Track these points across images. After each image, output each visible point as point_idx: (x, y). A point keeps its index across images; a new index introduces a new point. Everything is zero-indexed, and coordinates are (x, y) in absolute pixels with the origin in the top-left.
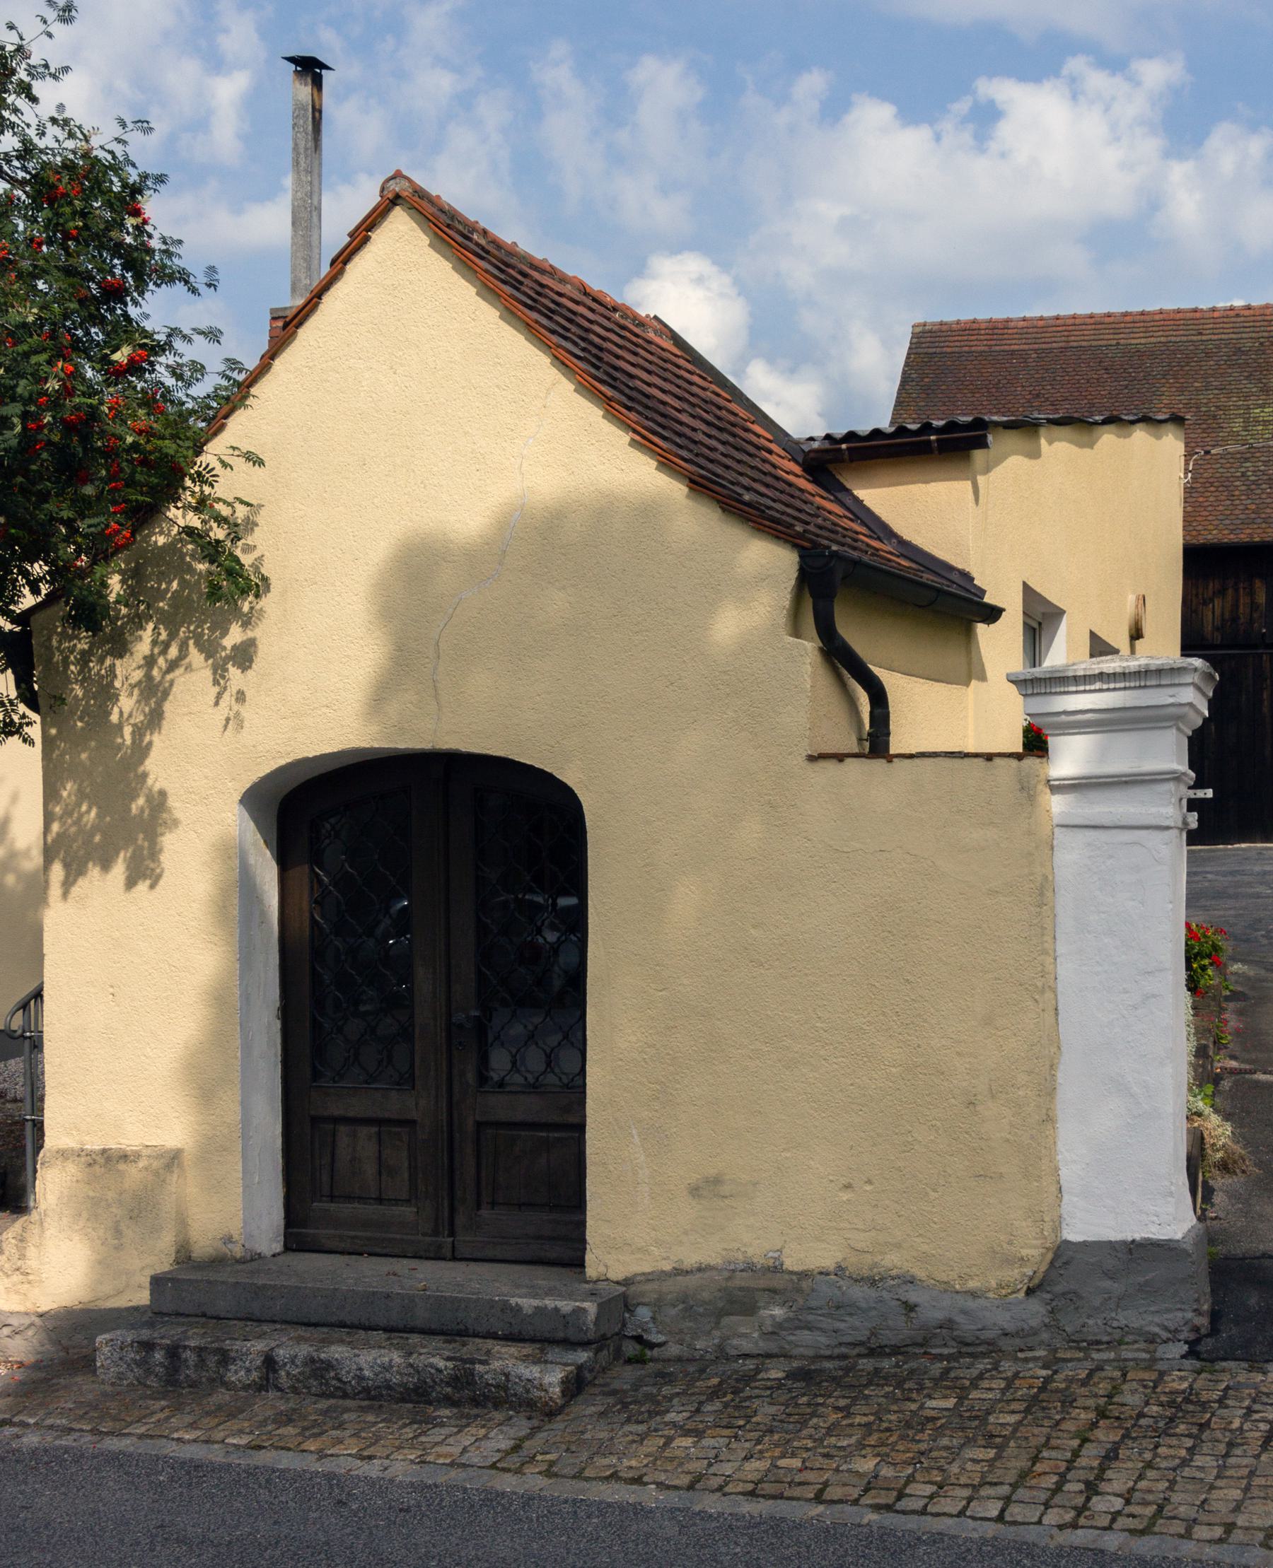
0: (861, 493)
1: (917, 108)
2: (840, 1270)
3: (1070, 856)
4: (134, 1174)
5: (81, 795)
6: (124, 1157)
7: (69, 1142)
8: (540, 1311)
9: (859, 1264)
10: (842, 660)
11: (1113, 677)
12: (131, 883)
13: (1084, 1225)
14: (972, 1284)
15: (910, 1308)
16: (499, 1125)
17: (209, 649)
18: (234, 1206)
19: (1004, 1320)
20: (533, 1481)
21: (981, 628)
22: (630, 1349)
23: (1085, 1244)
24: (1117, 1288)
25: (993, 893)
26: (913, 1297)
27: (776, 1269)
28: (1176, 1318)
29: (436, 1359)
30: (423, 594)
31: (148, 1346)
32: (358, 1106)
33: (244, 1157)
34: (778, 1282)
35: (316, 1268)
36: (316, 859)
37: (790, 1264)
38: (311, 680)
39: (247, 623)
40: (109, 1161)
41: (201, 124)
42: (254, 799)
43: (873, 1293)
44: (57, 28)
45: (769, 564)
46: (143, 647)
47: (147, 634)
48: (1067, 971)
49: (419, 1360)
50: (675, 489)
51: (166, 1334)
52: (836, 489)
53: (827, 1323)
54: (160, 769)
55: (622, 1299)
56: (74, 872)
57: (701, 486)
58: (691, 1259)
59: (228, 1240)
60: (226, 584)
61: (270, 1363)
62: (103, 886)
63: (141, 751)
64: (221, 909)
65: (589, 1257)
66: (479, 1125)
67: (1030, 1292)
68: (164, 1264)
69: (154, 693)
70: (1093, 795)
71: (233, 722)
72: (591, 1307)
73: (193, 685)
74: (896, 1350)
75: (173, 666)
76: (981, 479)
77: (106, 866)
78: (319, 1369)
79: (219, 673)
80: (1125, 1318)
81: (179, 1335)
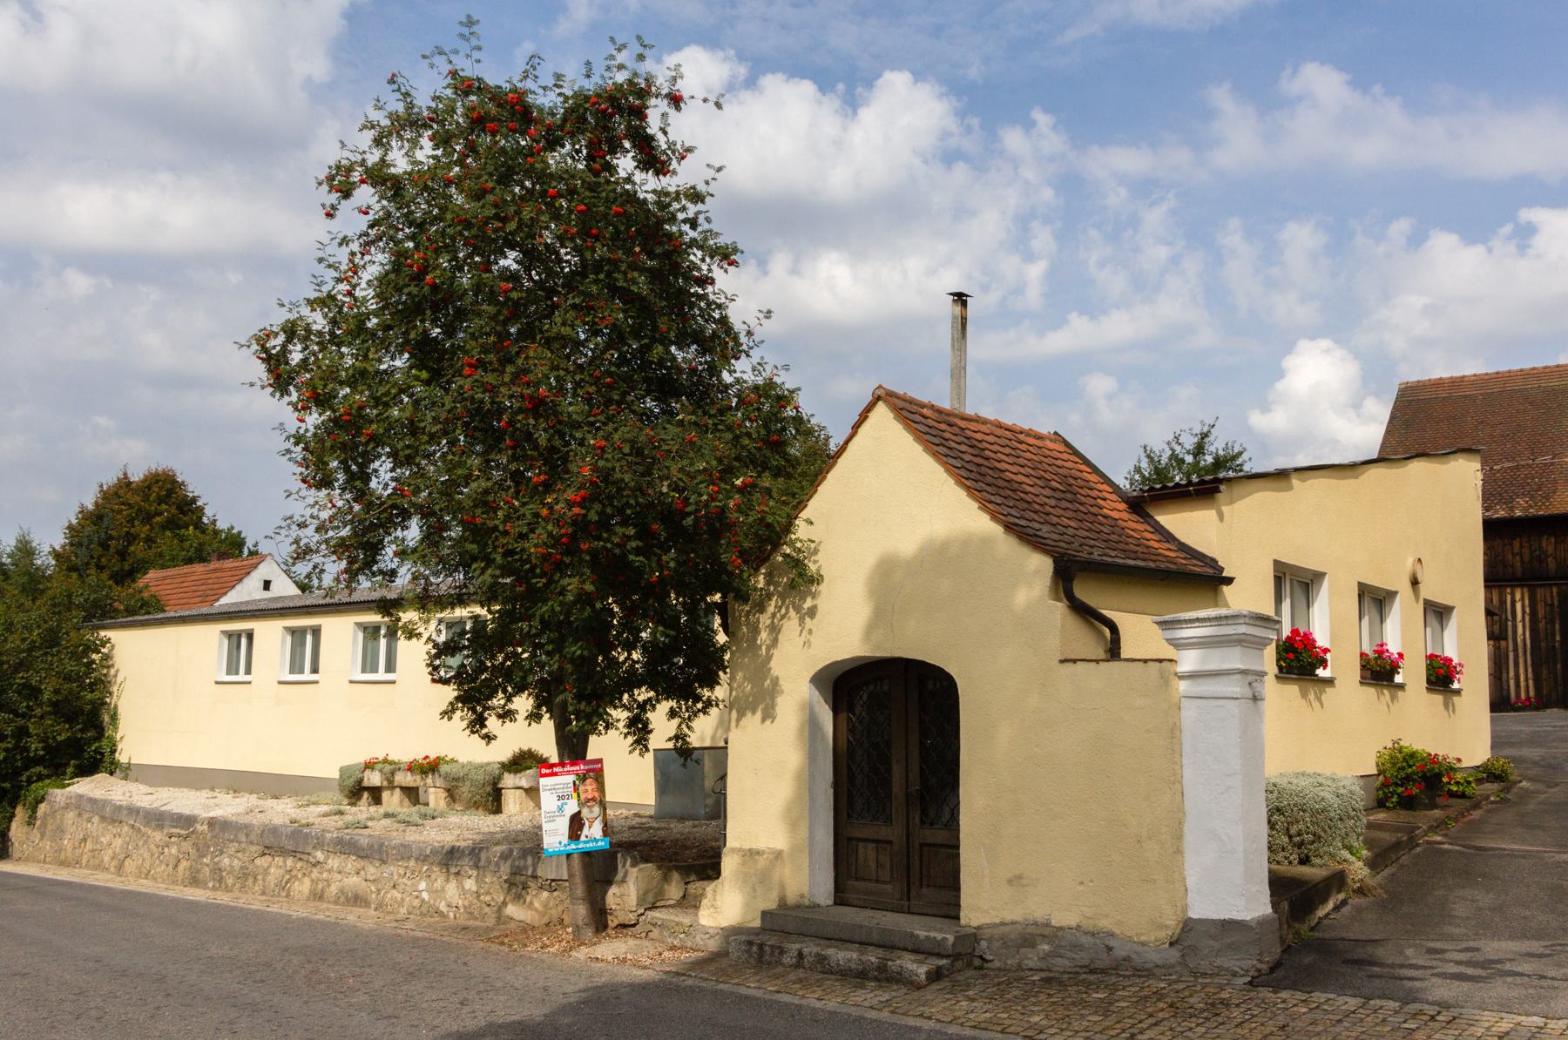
0: (1158, 518)
1: (1474, 232)
2: (1078, 927)
3: (1189, 713)
4: (762, 862)
5: (745, 678)
6: (758, 853)
7: (737, 845)
8: (927, 938)
9: (1088, 925)
10: (1083, 612)
11: (1204, 620)
12: (763, 720)
13: (1200, 909)
14: (1143, 938)
15: (1110, 949)
16: (930, 845)
17: (798, 609)
18: (807, 878)
19: (1156, 958)
20: (885, 1015)
21: (1225, 588)
22: (977, 962)
23: (1200, 920)
24: (1216, 945)
25: (1148, 731)
26: (1111, 944)
27: (1048, 925)
28: (1247, 964)
29: (873, 957)
30: (890, 584)
31: (750, 943)
32: (868, 832)
33: (810, 853)
34: (1046, 932)
35: (850, 915)
36: (851, 709)
37: (1054, 923)
38: (834, 625)
39: (814, 596)
40: (751, 854)
41: (1019, 290)
42: (818, 679)
43: (1091, 940)
44: (764, 321)
45: (1040, 565)
46: (771, 609)
47: (773, 603)
48: (1187, 773)
49: (865, 958)
50: (997, 529)
51: (764, 938)
52: (1147, 518)
53: (1069, 954)
54: (777, 667)
55: (974, 937)
56: (741, 715)
57: (1009, 528)
58: (1009, 916)
59: (802, 896)
60: (801, 580)
61: (800, 955)
62: (752, 721)
63: (769, 658)
64: (801, 730)
65: (962, 914)
66: (921, 845)
67: (1171, 944)
68: (771, 904)
69: (775, 630)
70: (1200, 681)
71: (807, 644)
72: (951, 938)
73: (791, 626)
74: (1103, 971)
75: (783, 617)
76: (1225, 509)
77: (754, 712)
78: (821, 959)
79: (802, 620)
80: (1219, 962)
81: (771, 940)
